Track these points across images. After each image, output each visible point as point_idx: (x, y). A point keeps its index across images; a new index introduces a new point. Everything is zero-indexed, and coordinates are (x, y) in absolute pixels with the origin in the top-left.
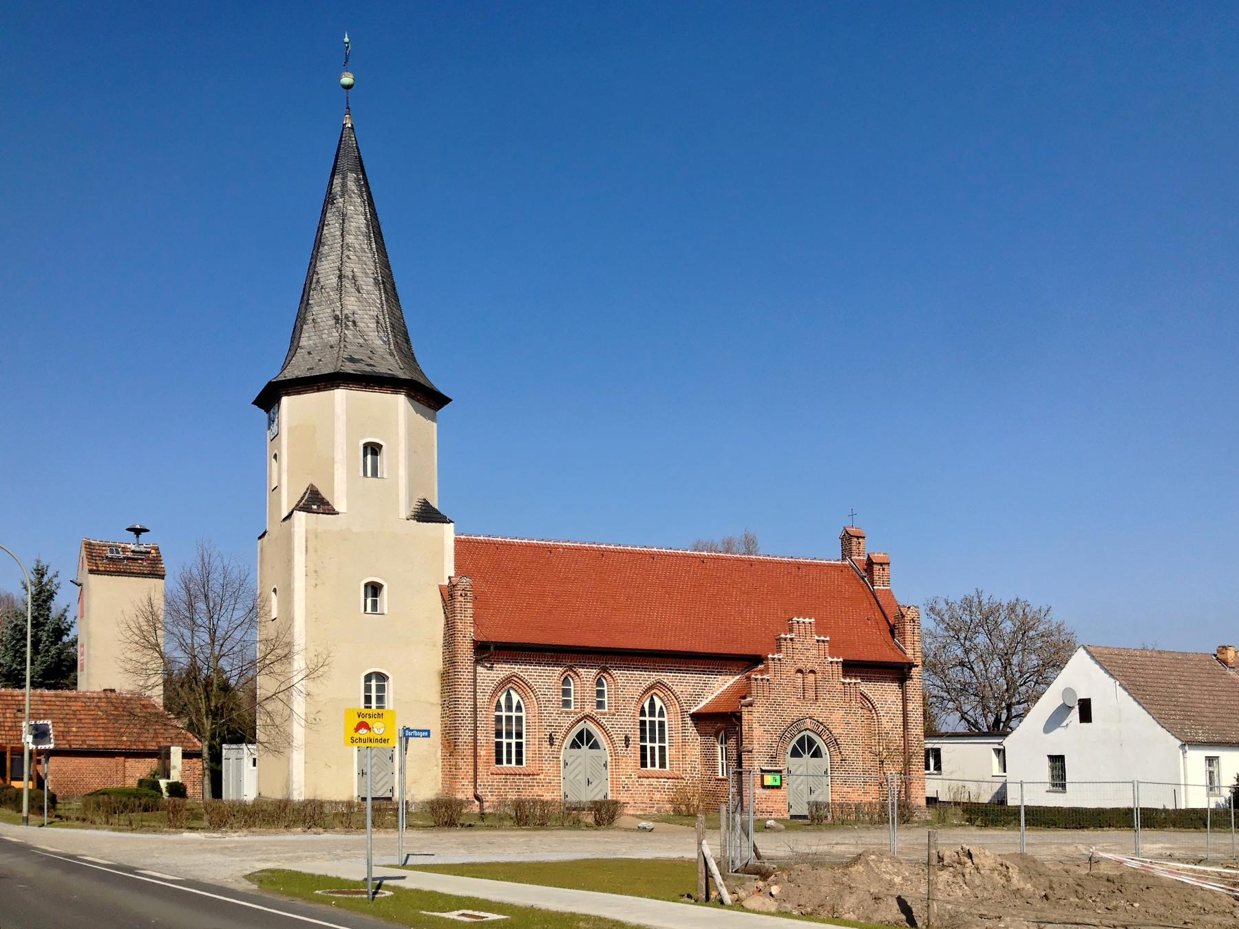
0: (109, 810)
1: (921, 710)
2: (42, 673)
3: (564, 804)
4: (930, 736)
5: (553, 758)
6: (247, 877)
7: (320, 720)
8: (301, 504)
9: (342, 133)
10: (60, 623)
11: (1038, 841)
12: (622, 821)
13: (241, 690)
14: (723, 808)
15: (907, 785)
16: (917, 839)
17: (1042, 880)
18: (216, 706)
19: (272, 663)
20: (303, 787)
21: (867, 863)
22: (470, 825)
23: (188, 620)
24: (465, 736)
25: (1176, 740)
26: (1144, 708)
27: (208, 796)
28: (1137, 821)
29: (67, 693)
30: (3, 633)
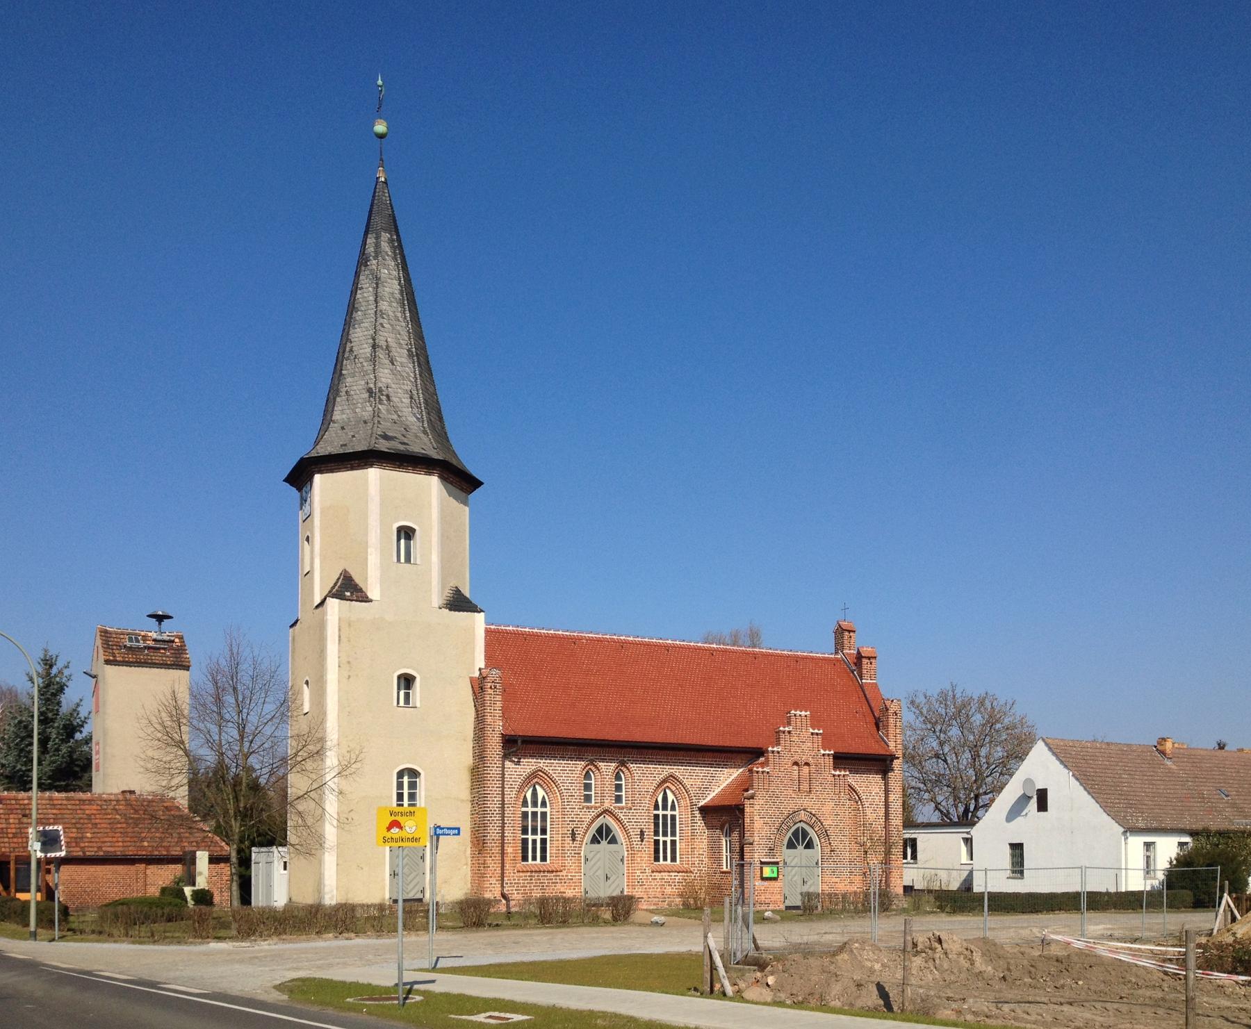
0: (129, 921)
1: (900, 801)
2: (51, 774)
3: (585, 901)
4: (907, 827)
5: (575, 853)
6: (279, 988)
7: (352, 819)
8: (334, 590)
9: (375, 188)
10: (72, 719)
11: (999, 926)
12: (638, 916)
13: (271, 789)
14: (727, 900)
15: (887, 873)
16: (894, 927)
17: (1001, 963)
18: (245, 807)
19: (304, 760)
20: (335, 891)
21: (852, 951)
22: (497, 925)
23: (215, 714)
24: (493, 833)
25: (1119, 826)
26: (1093, 797)
27: (236, 903)
28: (1084, 905)
29: (81, 795)
30: (5, 730)
